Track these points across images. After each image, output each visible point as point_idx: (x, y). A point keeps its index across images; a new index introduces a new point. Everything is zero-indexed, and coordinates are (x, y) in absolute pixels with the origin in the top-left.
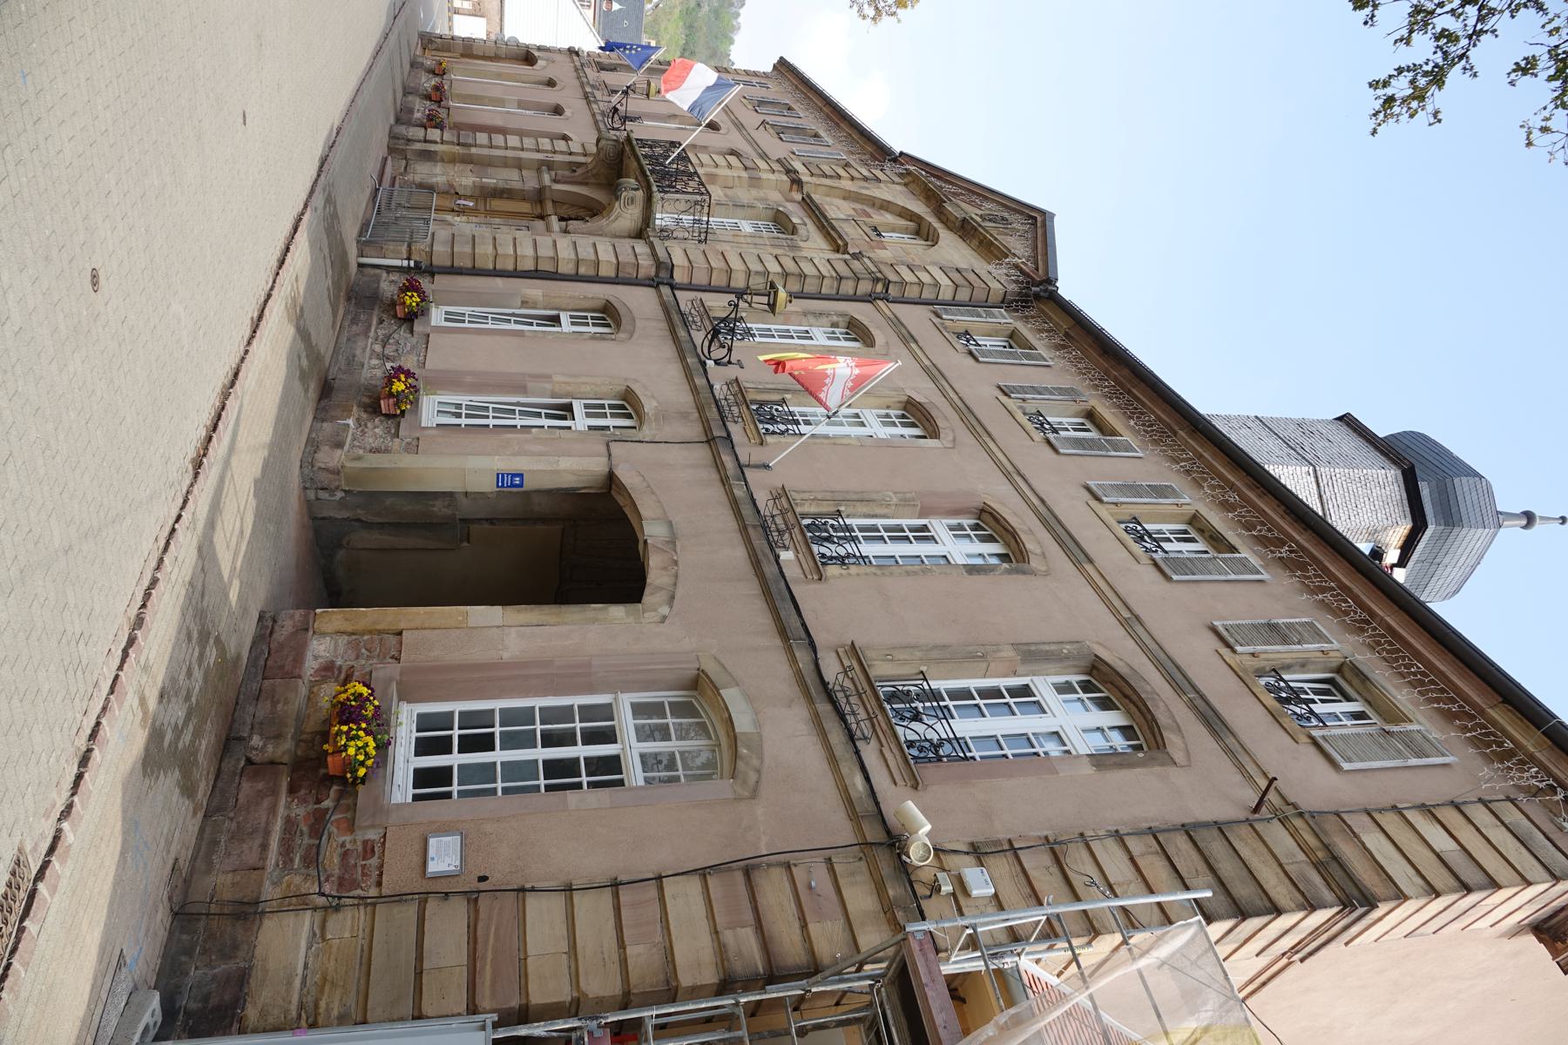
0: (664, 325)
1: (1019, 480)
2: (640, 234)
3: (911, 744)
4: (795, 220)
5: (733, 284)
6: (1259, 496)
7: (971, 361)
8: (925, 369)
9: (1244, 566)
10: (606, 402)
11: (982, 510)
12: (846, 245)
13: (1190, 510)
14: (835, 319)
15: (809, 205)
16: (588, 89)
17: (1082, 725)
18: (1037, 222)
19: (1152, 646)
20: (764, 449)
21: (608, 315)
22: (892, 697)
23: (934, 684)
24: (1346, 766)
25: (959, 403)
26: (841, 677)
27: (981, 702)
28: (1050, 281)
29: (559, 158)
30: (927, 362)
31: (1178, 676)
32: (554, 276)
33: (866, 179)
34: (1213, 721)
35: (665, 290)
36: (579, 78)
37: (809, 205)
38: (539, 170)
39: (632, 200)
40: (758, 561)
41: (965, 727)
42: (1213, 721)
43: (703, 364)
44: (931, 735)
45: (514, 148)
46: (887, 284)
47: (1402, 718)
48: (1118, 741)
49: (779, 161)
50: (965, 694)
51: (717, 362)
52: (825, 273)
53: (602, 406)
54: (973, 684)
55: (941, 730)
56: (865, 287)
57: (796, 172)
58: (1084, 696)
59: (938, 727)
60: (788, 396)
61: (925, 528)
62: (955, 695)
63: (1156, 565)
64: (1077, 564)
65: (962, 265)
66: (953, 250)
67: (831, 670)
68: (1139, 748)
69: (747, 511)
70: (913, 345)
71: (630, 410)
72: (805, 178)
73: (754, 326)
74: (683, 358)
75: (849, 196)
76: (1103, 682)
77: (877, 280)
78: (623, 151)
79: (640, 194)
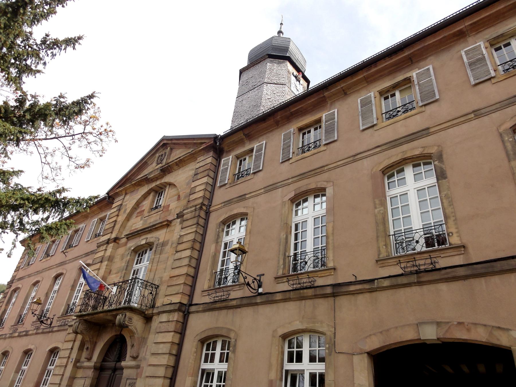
0: (224, 312)
1: (359, 156)
2: (148, 319)
3: (234, 282)
4: (143, 242)
5: (192, 274)
6: (376, 67)
7: (260, 174)
8: (266, 192)
9: (259, 150)
10: (204, 352)
11: (383, 172)
12: (167, 221)
13: (377, 94)
14: (221, 229)
15: (131, 236)
16: (17, 334)
17: (312, 211)
18: (166, 144)
19: (498, 106)
20: (338, 266)
21: (207, 342)
22: (219, 284)
23: (219, 270)
24: (261, 169)
25: (299, 177)
26: (210, 297)
27: (226, 258)
28: (215, 138)
29: (74, 356)
30: (262, 191)
31: (408, 138)
32: (175, 368)
33: (119, 210)
34: (242, 198)
35: (193, 309)
36: (5, 338)
37: (131, 236)
38: (78, 368)
39: (130, 319)
40: (448, 278)
41: (309, 247)
42: (242, 198)
43: (260, 294)
44: (312, 259)
45: (61, 380)
46: (202, 204)
47: (319, 121)
48: (244, 223)
49: (98, 247)
50: (223, 262)
51: (260, 286)
52: (194, 230)
53: (52, 360)
54: (221, 259)
55: (231, 271)
56: (203, 214)
57: (109, 240)
58: (231, 228)
59: (230, 272)
60: (214, 271)
61: (134, 271)
62: (223, 265)
63: (425, 105)
64: (428, 135)
65: (192, 173)
66: (180, 177)
67: (285, 287)
68: (247, 218)
69: (287, 295)
70: (247, 196)
71: (212, 341)
72: (114, 236)
73: (73, 301)
74: (256, 304)
75: (128, 218)
76: (299, 199)
77: (201, 208)
78: (86, 321)
79: (128, 314)
